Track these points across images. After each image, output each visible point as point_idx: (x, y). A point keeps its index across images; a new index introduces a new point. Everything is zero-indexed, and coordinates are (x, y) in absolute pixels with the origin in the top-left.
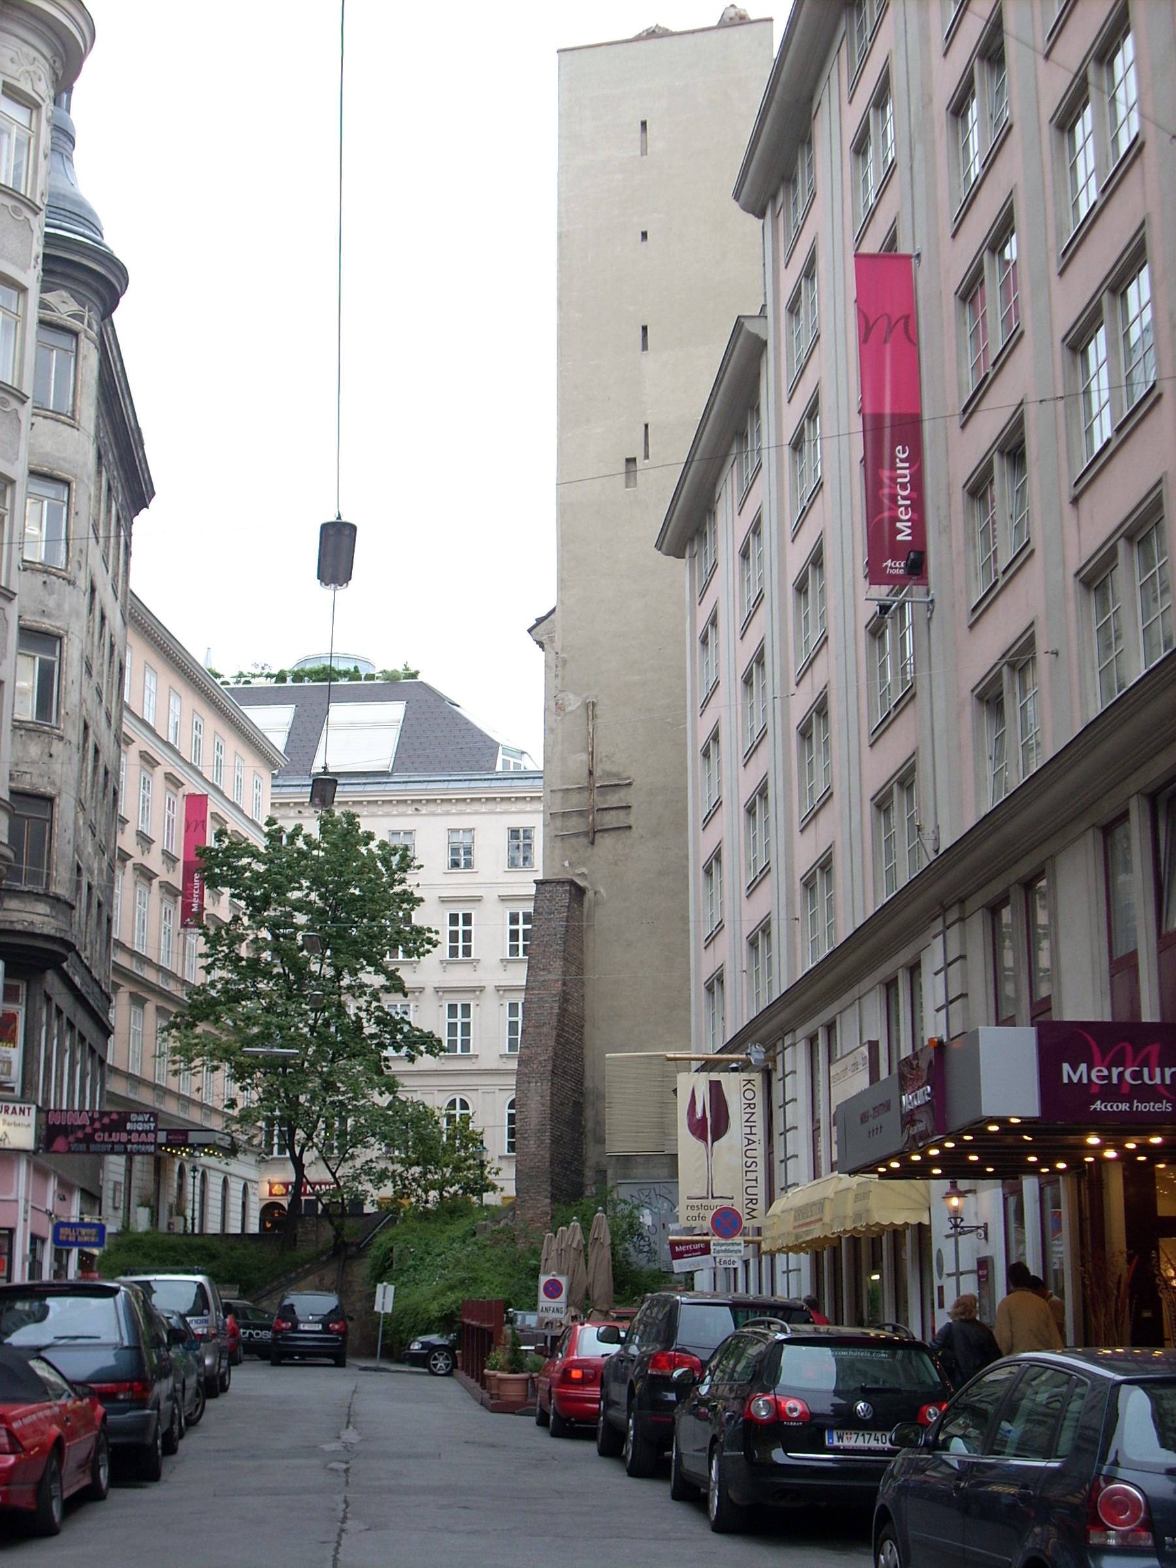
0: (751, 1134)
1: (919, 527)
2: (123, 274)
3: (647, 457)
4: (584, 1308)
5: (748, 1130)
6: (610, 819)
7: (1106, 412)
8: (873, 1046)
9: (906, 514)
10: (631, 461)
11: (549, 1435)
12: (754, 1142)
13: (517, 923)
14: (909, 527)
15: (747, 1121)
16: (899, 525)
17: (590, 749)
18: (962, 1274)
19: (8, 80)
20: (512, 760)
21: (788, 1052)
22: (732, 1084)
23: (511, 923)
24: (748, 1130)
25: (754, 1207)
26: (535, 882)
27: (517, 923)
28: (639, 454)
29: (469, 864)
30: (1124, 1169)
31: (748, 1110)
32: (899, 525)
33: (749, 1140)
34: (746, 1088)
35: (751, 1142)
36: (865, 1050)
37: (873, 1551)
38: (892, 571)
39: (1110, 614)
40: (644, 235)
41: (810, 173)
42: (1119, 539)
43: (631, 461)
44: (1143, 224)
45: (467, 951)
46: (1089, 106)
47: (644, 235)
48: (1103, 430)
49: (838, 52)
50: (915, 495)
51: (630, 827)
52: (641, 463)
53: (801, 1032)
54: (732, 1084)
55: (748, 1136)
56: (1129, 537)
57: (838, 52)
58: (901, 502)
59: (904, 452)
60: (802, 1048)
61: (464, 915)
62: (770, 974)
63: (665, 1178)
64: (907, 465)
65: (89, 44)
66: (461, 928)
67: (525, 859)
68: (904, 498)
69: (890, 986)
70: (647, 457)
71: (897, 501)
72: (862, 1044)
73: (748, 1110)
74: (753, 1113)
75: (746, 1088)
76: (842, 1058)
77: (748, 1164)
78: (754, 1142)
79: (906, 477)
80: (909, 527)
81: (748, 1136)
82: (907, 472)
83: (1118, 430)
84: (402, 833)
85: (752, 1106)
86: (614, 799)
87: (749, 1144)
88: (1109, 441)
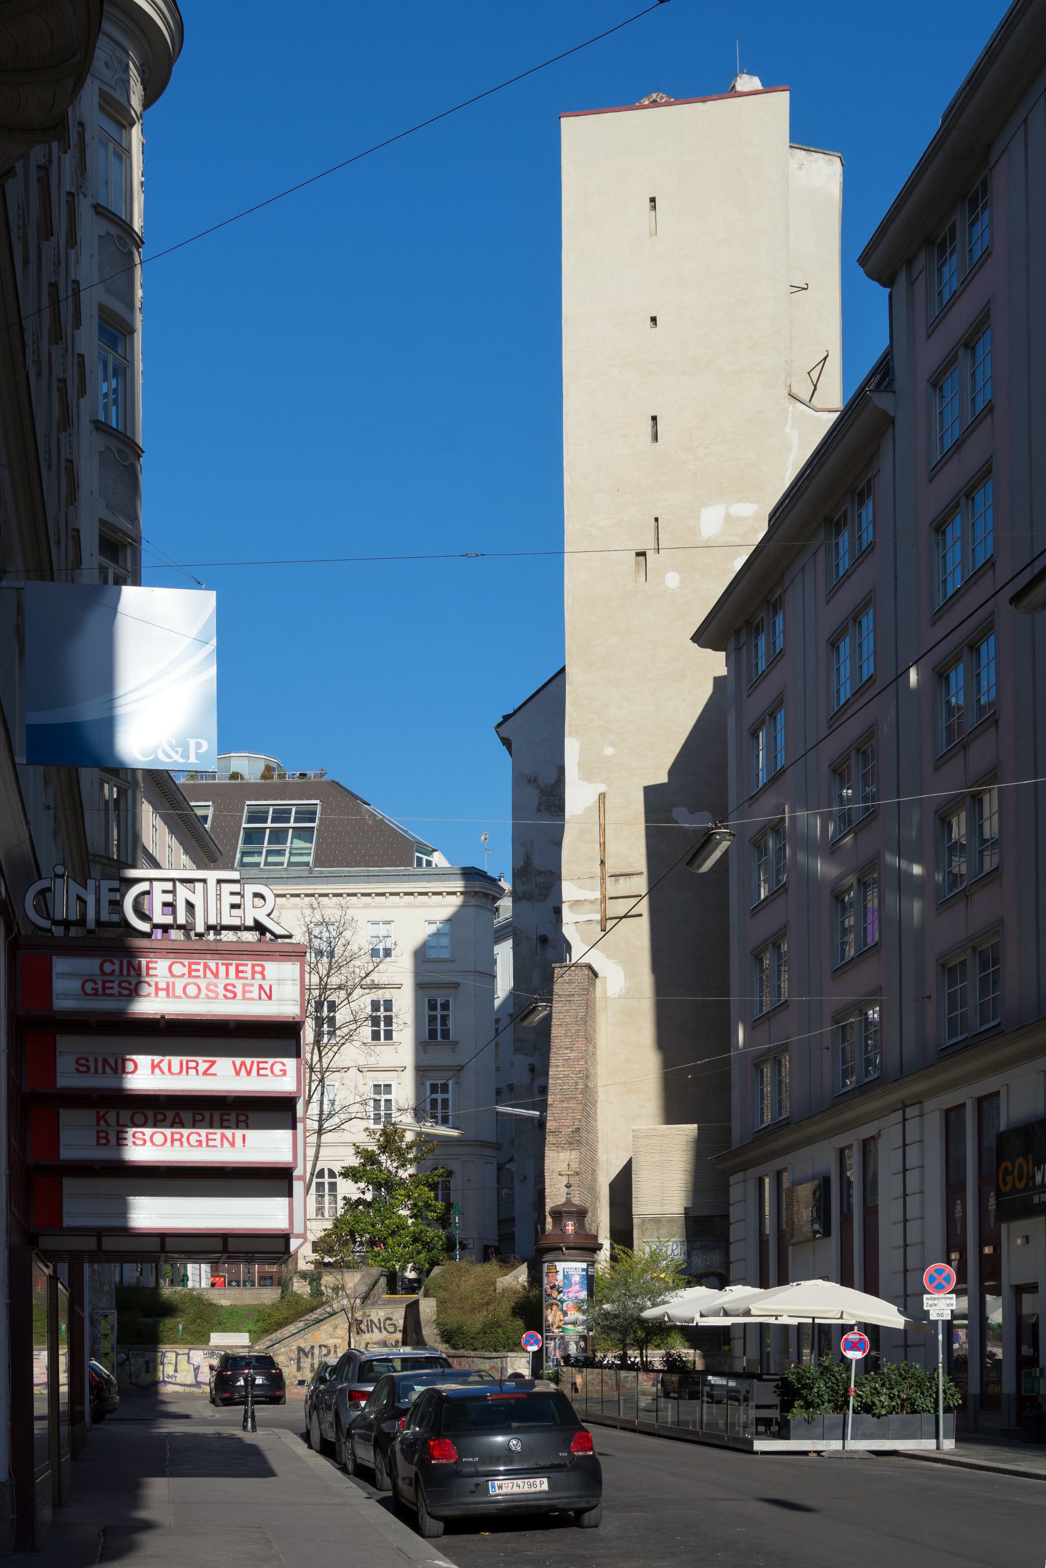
2: (124, 230)
4: (408, 1227)
7: (848, 684)
11: (684, 1205)
18: (907, 1106)
19: (105, 88)
20: (425, 857)
30: (135, 1125)
39: (979, 209)
42: (960, 347)
44: (989, 302)
45: (446, 1034)
46: (955, 255)
48: (846, 693)
56: (966, 346)
65: (176, 54)
66: (439, 1013)
83: (854, 695)
84: (381, 923)
88: (849, 699)
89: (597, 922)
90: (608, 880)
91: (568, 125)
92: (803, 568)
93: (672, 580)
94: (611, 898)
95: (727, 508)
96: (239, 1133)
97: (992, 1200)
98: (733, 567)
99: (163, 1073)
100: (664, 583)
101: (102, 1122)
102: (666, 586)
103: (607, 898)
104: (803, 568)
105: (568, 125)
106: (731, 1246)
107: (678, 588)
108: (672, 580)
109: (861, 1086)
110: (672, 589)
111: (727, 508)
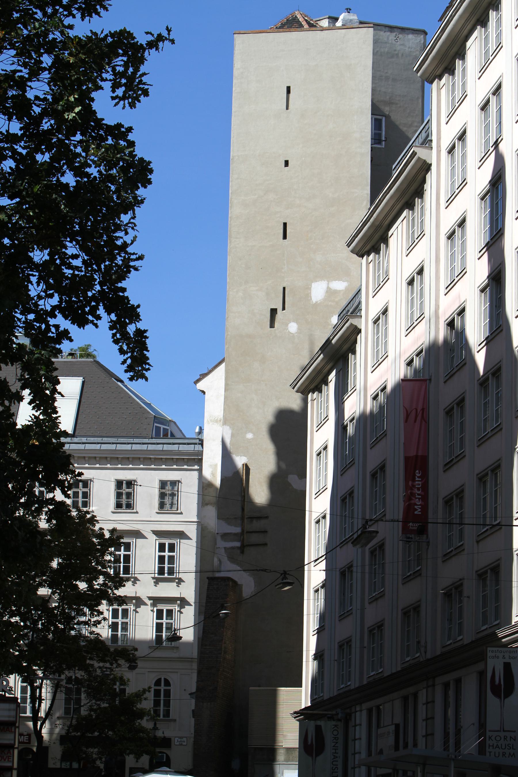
0: (335, 753)
1: (425, 508)
3: (284, 309)
5: (334, 751)
6: (254, 539)
8: (397, 726)
9: (419, 502)
10: (274, 312)
12: (337, 757)
13: (169, 557)
14: (419, 508)
15: (334, 746)
16: (416, 507)
17: (243, 494)
21: (358, 714)
22: (327, 726)
23: (160, 551)
24: (334, 751)
25: (337, 741)
26: (208, 578)
27: (169, 557)
28: (279, 307)
29: (129, 506)
31: (335, 741)
32: (416, 507)
33: (496, 747)
34: (334, 729)
35: (335, 757)
36: (393, 728)
37: (63, 716)
38: (412, 528)
40: (287, 163)
41: (386, 324)
43: (274, 312)
47: (287, 163)
49: (402, 221)
50: (423, 494)
51: (265, 544)
52: (280, 313)
53: (365, 706)
54: (327, 726)
55: (334, 754)
57: (402, 221)
58: (417, 497)
59: (419, 474)
60: (364, 713)
61: (167, 610)
62: (326, 470)
63: (283, 762)
64: (420, 479)
67: (172, 504)
68: (418, 495)
69: (405, 699)
70: (284, 309)
71: (416, 496)
72: (392, 724)
73: (335, 741)
74: (337, 743)
75: (334, 729)
76: (384, 727)
77: (334, 769)
78: (337, 757)
79: (419, 485)
80: (419, 508)
81: (334, 754)
82: (420, 483)
85: (337, 739)
86: (257, 525)
87: (499, 747)
89: (238, 547)
90: (246, 520)
91: (239, 39)
92: (397, 227)
93: (293, 327)
94: (247, 532)
95: (328, 284)
96: (394, 735)
97: (37, 705)
98: (331, 322)
99: (333, 728)
100: (288, 329)
101: (334, 726)
102: (289, 332)
103: (245, 532)
104: (397, 227)
105: (239, 39)
106: (53, 305)
107: (296, 333)
108: (293, 327)
109: (347, 686)
110: (293, 334)
111: (328, 284)
